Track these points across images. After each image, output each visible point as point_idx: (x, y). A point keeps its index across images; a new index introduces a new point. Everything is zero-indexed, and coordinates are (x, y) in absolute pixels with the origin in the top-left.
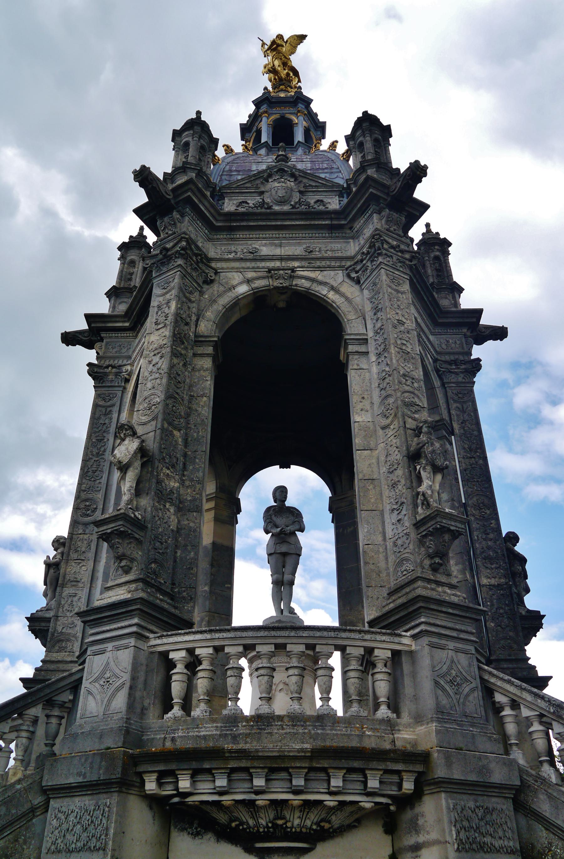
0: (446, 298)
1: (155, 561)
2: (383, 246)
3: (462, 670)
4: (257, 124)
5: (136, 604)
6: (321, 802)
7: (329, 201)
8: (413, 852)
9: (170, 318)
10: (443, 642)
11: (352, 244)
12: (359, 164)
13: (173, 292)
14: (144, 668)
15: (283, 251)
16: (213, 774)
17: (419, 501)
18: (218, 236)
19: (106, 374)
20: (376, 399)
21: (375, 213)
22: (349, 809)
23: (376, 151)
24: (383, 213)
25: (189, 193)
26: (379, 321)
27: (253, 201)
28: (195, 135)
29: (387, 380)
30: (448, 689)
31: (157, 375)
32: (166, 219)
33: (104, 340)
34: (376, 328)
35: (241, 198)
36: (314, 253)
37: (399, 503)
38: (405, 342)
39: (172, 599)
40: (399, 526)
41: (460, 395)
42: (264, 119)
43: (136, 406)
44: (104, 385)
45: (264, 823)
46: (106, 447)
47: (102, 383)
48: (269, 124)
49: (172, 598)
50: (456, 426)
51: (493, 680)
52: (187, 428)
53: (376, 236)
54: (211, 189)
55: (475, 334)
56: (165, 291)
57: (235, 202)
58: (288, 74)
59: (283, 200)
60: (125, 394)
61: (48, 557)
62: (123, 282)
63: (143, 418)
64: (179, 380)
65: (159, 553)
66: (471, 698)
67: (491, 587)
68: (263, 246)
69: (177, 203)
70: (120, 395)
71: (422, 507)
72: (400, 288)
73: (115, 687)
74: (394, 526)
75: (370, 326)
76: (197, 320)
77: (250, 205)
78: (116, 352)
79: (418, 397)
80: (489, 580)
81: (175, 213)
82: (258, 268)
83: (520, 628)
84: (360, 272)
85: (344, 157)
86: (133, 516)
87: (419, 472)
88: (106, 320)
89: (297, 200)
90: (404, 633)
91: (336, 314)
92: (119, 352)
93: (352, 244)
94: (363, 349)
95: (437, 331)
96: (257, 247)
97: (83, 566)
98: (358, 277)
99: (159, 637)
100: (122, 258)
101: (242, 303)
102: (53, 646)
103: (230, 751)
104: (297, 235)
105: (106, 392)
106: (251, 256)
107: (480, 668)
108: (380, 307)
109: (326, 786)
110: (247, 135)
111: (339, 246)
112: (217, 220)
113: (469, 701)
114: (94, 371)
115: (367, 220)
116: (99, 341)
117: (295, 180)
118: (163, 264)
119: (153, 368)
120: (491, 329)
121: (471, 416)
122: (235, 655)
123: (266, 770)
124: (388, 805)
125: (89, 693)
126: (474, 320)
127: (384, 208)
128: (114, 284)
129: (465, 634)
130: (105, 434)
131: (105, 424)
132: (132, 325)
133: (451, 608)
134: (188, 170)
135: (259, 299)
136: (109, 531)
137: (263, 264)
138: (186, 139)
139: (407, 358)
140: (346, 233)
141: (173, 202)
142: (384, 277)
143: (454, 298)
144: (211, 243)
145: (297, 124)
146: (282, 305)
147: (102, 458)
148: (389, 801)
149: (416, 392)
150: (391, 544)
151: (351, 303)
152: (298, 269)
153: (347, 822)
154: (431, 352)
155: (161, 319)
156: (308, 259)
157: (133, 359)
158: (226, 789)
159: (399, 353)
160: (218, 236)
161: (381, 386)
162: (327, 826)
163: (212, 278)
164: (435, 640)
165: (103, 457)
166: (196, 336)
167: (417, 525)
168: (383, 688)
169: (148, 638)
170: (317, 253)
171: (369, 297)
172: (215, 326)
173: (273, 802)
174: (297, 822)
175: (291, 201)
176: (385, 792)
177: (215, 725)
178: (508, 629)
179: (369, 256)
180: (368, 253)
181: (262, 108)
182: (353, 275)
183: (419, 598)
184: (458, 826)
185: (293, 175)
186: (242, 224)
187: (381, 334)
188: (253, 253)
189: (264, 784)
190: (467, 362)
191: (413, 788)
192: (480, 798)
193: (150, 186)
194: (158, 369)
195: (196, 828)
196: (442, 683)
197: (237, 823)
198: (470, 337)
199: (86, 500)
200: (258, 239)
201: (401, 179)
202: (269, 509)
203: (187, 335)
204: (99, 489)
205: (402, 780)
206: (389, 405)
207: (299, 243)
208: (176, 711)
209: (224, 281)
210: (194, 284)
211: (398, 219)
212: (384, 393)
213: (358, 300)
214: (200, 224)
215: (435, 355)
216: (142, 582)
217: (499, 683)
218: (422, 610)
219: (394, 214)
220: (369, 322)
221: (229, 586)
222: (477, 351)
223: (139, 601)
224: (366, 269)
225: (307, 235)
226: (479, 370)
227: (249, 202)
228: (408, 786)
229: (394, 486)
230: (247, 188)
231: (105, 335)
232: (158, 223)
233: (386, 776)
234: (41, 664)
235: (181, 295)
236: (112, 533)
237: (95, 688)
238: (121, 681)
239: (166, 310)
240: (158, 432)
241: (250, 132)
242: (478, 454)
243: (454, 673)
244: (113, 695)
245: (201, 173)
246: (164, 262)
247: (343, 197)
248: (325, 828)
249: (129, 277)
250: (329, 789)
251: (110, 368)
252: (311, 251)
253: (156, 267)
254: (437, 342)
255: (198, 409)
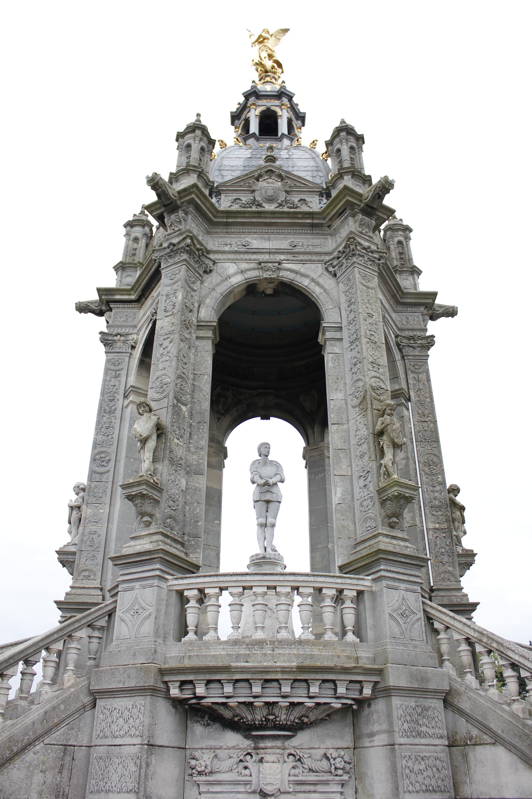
0: (407, 279)
1: (170, 517)
2: (356, 247)
3: (410, 605)
4: (245, 113)
5: (157, 553)
6: (302, 703)
7: (311, 199)
8: (369, 737)
9: (178, 306)
10: (396, 584)
11: (330, 240)
12: (337, 171)
13: (179, 283)
14: (165, 602)
15: (271, 245)
16: (222, 683)
17: (382, 472)
18: (216, 230)
19: (114, 341)
20: (348, 380)
21: (350, 216)
22: (323, 708)
23: (351, 158)
24: (356, 218)
25: (193, 196)
26: (352, 312)
27: (245, 198)
28: (195, 135)
29: (358, 366)
30: (399, 620)
31: (167, 358)
32: (173, 217)
33: (113, 310)
34: (349, 319)
35: (235, 196)
36: (298, 247)
37: (366, 472)
38: (373, 333)
39: (183, 547)
40: (365, 490)
41: (417, 367)
42: (252, 111)
43: (150, 383)
44: (113, 351)
45: (259, 718)
46: (116, 406)
47: (112, 349)
48: (256, 116)
49: (183, 545)
50: (412, 394)
51: (433, 612)
52: (193, 403)
53: (351, 239)
54: (210, 187)
55: (431, 312)
56: (172, 281)
57: (230, 198)
58: (273, 67)
59: (271, 198)
60: (132, 359)
61: (71, 501)
62: (128, 257)
63: (156, 395)
64: (185, 361)
65: (172, 510)
66: (416, 626)
67: (436, 531)
68: (255, 239)
69: (182, 203)
70: (128, 360)
71: (384, 477)
72: (369, 284)
73: (143, 616)
74: (361, 490)
75: (344, 316)
76: (199, 306)
77: (243, 202)
78: (123, 321)
79: (383, 381)
80: (434, 525)
81: (180, 212)
82: (250, 260)
83: (457, 564)
84: (337, 267)
85: (324, 157)
86: (152, 481)
87: (382, 447)
88: (113, 293)
89: (283, 199)
90: (367, 578)
91: (316, 302)
92: (126, 320)
93: (330, 240)
94: (338, 335)
95: (399, 309)
96: (249, 240)
97: (101, 509)
98: (334, 271)
99: (176, 579)
100: (127, 235)
101: (236, 291)
102: (79, 575)
103: (236, 668)
104: (283, 231)
105: (116, 357)
106: (243, 249)
107: (423, 603)
108: (353, 300)
109: (306, 692)
110: (236, 122)
111: (319, 241)
112: (215, 217)
113: (414, 628)
114: (106, 340)
115: (343, 222)
116: (108, 311)
117: (282, 180)
118: (170, 256)
119: (163, 351)
120: (444, 308)
121: (425, 385)
122: (237, 594)
123: (262, 681)
124: (352, 705)
125: (122, 620)
126: (430, 301)
127: (358, 213)
128: (121, 260)
129: (413, 577)
130: (115, 395)
131: (115, 386)
132: (137, 298)
133: (404, 558)
134: (190, 172)
135: (251, 289)
136: (134, 493)
137: (254, 257)
138: (188, 141)
139: (375, 347)
140: (324, 231)
141: (178, 202)
142: (357, 275)
143: (414, 279)
144: (210, 235)
145: (281, 116)
146: (269, 291)
147: (114, 416)
148: (353, 702)
149: (381, 377)
150: (358, 504)
151: (329, 295)
152: (284, 262)
153: (321, 717)
154: (394, 329)
155: (170, 308)
156: (292, 252)
157: (138, 328)
158: (232, 694)
159: (368, 343)
160: (216, 230)
161: (353, 370)
162: (306, 720)
163: (211, 269)
164: (391, 583)
165: (114, 415)
166: (198, 321)
167: (380, 491)
168: (350, 619)
169: (167, 579)
170: (300, 247)
171: (343, 290)
172: (214, 312)
173: (267, 703)
174: (283, 717)
175: (278, 199)
176: (350, 696)
177: (221, 647)
178: (448, 564)
179: (344, 255)
180: (344, 252)
181: (250, 100)
182: (331, 269)
183: (379, 551)
184: (402, 719)
185: (280, 176)
186: (236, 220)
187: (354, 325)
188: (246, 246)
189: (260, 691)
190: (423, 338)
191: (370, 693)
192: (421, 700)
193: (160, 190)
194: (168, 353)
195: (207, 721)
196: (395, 615)
197: (239, 718)
198: (427, 315)
199: (102, 452)
200: (250, 233)
201: (373, 190)
202: (254, 462)
203: (191, 321)
204: (112, 443)
205: (362, 687)
206: (359, 388)
207: (285, 237)
208: (191, 636)
209: (221, 270)
210: (196, 274)
211: (370, 223)
212: (355, 377)
213: (334, 292)
214: (201, 220)
215: (397, 331)
216: (161, 535)
217: (438, 614)
218: (381, 560)
219: (366, 218)
220: (343, 312)
221: (218, 522)
222: (433, 327)
223: (160, 551)
224: (342, 265)
225: (292, 231)
226: (432, 346)
227: (242, 198)
228: (367, 691)
229: (362, 456)
230: (241, 186)
231: (113, 306)
232: (166, 220)
233: (351, 684)
234: (70, 589)
235: (186, 286)
236: (136, 494)
237: (127, 617)
238: (148, 613)
239: (174, 299)
240: (170, 408)
241: (239, 119)
242: (430, 418)
243: (404, 608)
244: (142, 623)
245: (201, 175)
246: (171, 256)
247: (323, 197)
248: (305, 721)
249: (134, 252)
250: (308, 694)
251: (119, 336)
252: (295, 246)
253: (164, 260)
254: (398, 319)
255: (200, 385)
